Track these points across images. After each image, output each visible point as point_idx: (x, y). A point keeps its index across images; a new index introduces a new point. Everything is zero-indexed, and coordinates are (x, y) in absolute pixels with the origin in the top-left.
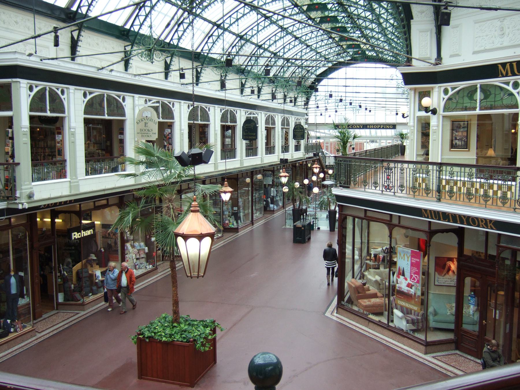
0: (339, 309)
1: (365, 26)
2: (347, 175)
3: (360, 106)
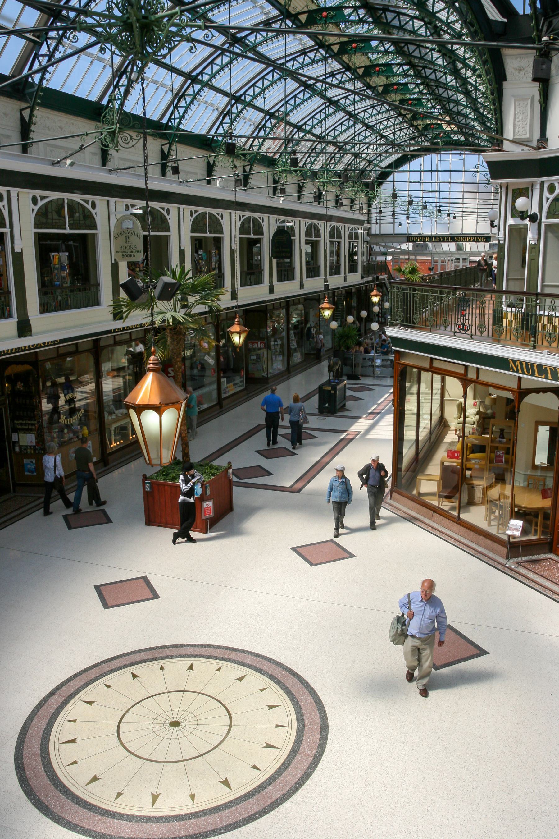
1: (447, 96)
2: (410, 307)
3: (439, 211)
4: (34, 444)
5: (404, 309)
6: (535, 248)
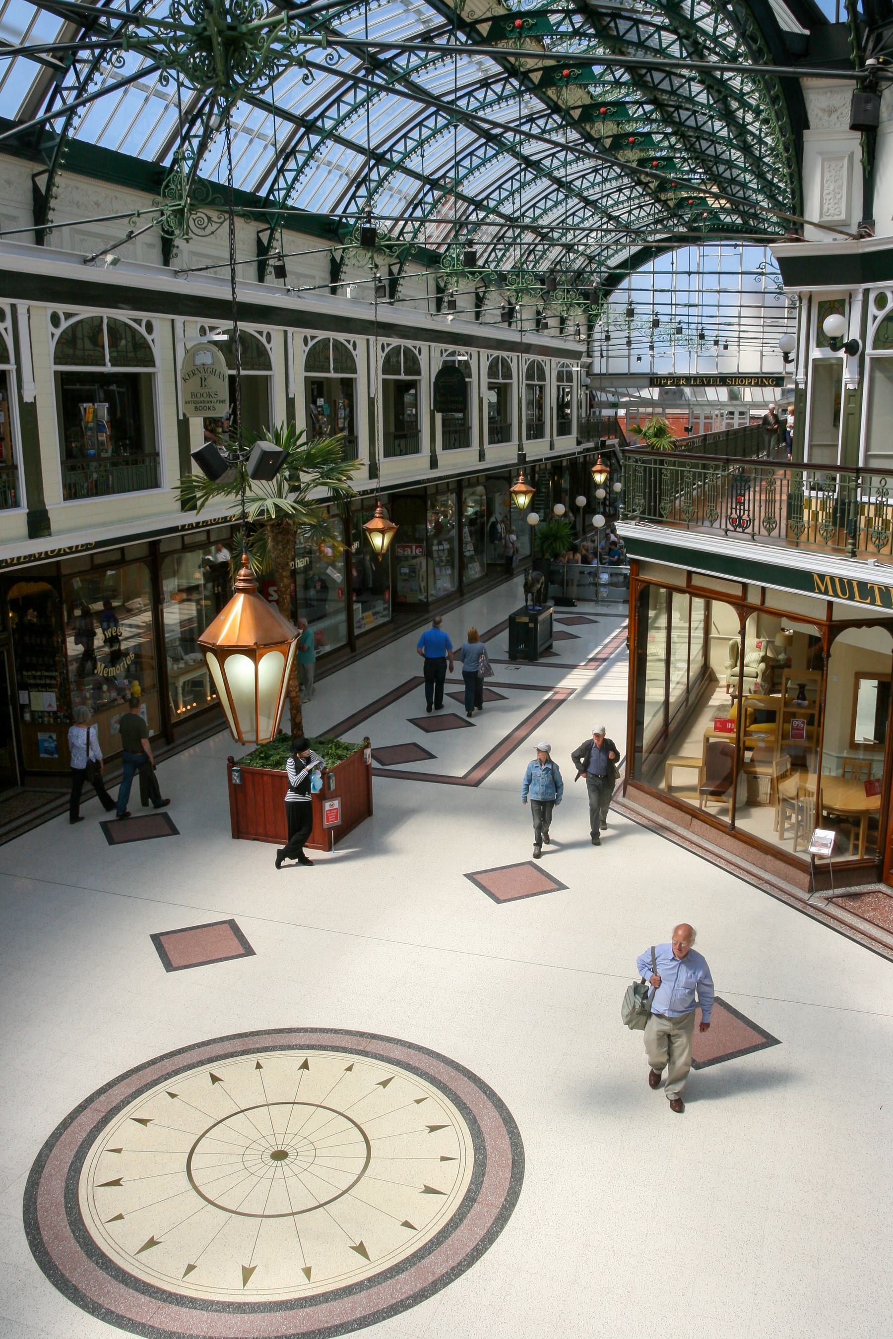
0: (629, 788)
1: (714, 154)
2: (655, 490)
3: (702, 337)
4: (55, 709)
5: (645, 493)
6: (854, 395)
